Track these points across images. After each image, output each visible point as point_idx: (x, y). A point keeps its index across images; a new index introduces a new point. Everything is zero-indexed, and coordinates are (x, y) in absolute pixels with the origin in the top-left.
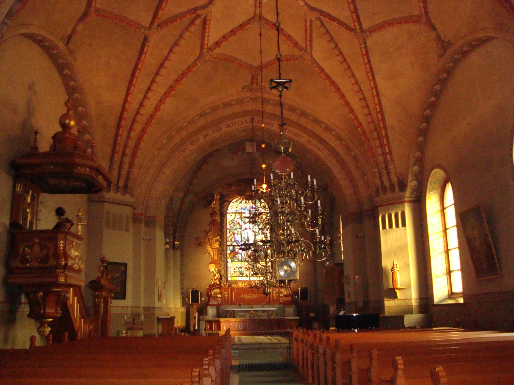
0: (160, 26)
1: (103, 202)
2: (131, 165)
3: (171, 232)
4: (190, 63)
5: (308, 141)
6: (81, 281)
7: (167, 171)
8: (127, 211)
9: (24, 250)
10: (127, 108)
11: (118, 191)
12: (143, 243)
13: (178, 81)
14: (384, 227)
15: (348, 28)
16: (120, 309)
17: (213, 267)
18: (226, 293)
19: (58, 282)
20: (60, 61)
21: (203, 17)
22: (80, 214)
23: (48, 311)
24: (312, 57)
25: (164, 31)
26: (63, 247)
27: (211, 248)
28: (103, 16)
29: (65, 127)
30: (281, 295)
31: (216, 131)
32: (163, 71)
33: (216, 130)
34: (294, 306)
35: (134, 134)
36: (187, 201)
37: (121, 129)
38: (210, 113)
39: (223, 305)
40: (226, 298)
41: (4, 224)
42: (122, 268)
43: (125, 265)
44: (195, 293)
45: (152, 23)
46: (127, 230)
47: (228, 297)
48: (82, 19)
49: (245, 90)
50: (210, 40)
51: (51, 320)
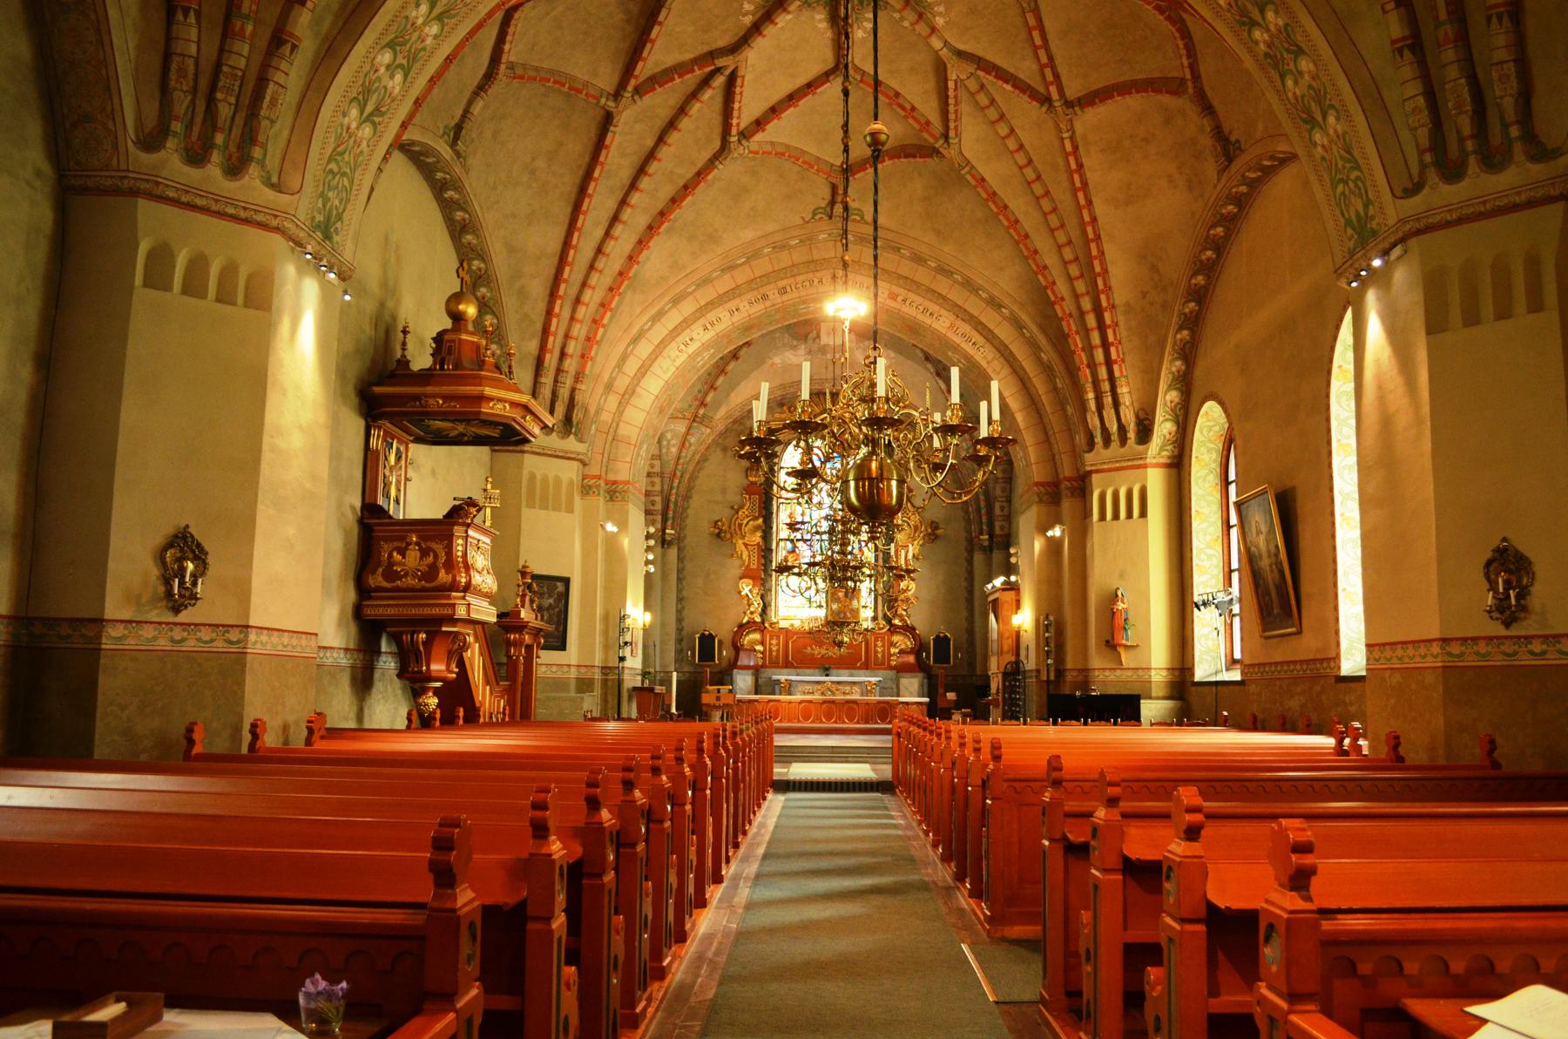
0: (639, 91)
3: (659, 507)
4: (700, 164)
5: (952, 325)
6: (486, 612)
9: (390, 556)
10: (570, 259)
13: (675, 201)
14: (1102, 517)
15: (1034, 95)
16: (554, 669)
17: (747, 586)
18: (774, 642)
19: (454, 614)
20: (439, 175)
21: (727, 72)
22: (489, 486)
23: (434, 667)
24: (961, 153)
25: (648, 100)
27: (746, 545)
28: (522, 77)
29: (457, 318)
30: (893, 650)
32: (645, 183)
34: (921, 675)
36: (693, 440)
37: (559, 302)
38: (743, 264)
39: (766, 667)
40: (774, 654)
41: (352, 507)
42: (560, 587)
43: (566, 581)
44: (707, 641)
45: (622, 85)
46: (570, 510)
47: (778, 650)
48: (481, 88)
49: (817, 217)
50: (743, 116)
51: (438, 684)
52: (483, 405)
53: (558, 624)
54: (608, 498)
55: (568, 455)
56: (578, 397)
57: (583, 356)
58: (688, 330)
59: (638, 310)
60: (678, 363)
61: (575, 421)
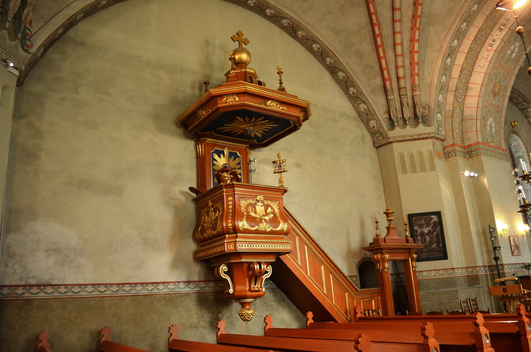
1: (391, 143)
8: (427, 146)
16: (442, 272)
26: (232, 209)
43: (438, 214)
46: (433, 169)
52: (219, 102)
53: (438, 242)
54: (468, 156)
55: (422, 136)
56: (417, 100)
58: (490, 36)
59: (444, 36)
60: (489, 59)
61: (419, 115)
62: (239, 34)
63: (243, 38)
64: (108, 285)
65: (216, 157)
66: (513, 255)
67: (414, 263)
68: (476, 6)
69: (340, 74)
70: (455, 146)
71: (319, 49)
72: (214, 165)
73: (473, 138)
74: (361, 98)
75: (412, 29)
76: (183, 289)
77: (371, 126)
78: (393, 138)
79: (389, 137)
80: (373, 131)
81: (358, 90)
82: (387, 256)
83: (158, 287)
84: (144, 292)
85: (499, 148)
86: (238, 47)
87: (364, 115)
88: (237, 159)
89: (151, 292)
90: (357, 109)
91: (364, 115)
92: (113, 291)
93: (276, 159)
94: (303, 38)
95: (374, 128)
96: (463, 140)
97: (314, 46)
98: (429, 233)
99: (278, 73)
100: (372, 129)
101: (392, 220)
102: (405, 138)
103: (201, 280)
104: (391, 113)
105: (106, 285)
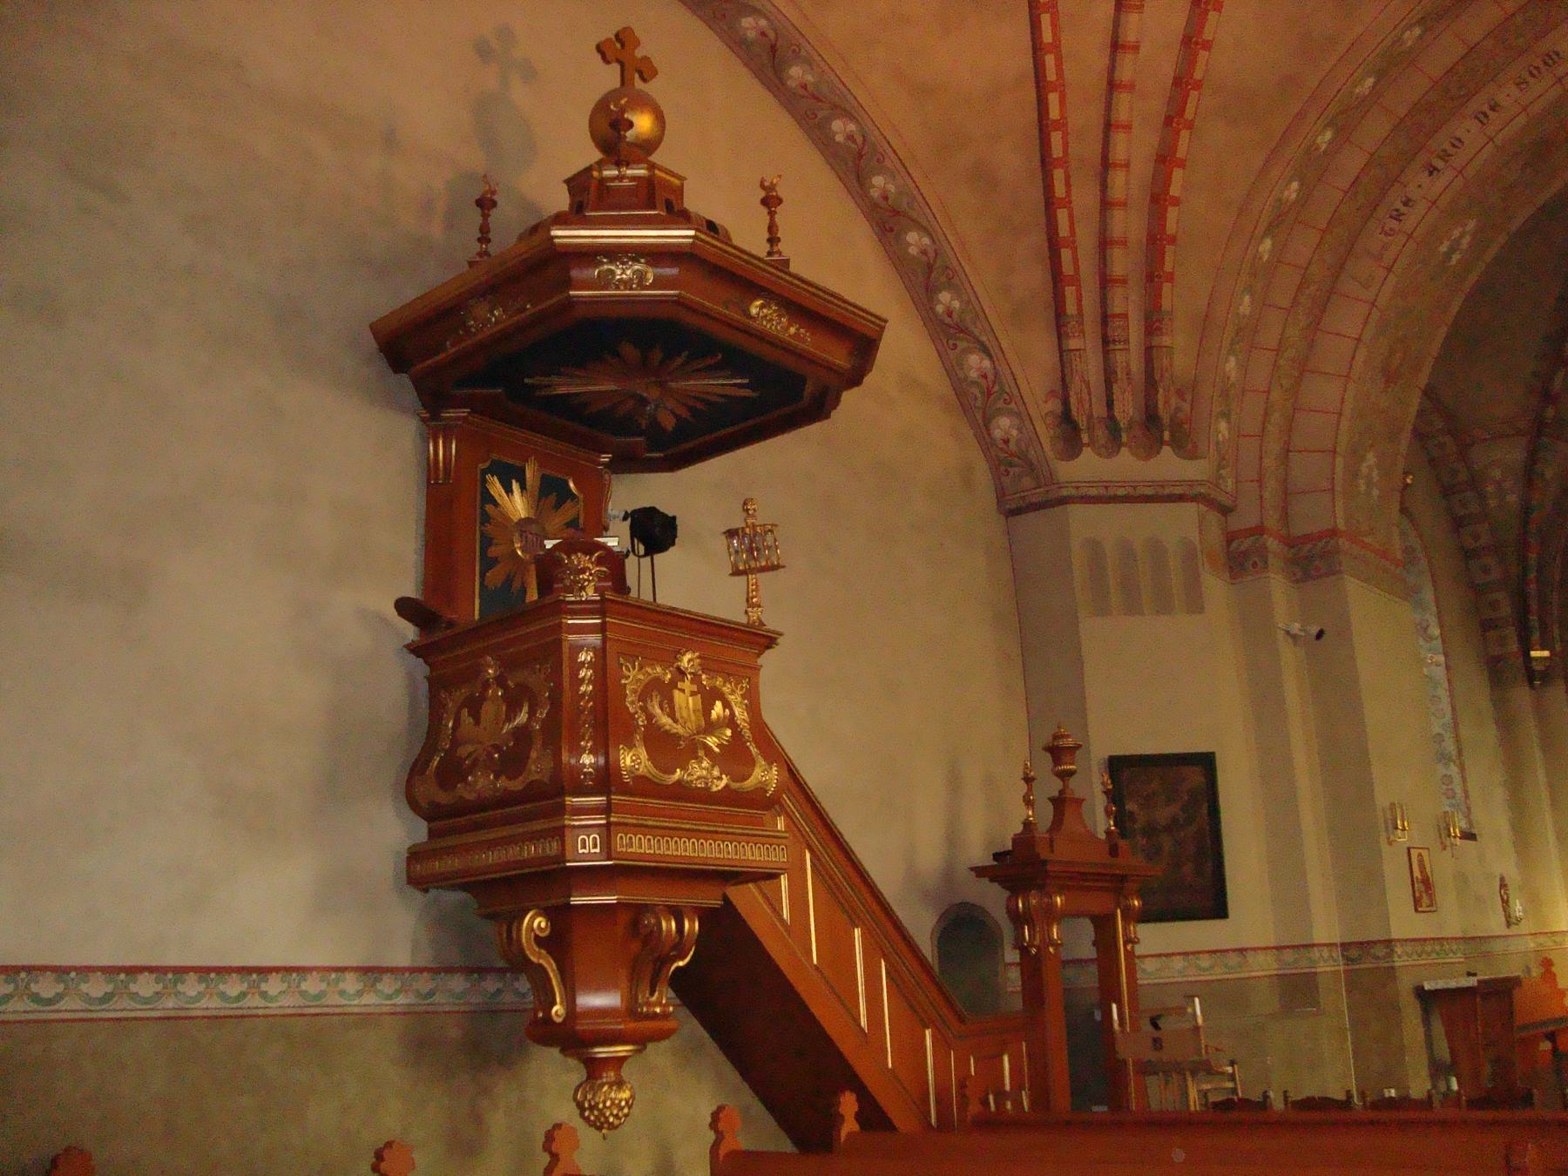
2: (1153, 324)
7: (1347, 320)
11: (1120, 445)
12: (1289, 656)
16: (1205, 962)
31: (1532, 75)
33: (1531, 73)
35: (1129, 184)
42: (1195, 777)
43: (1206, 762)
46: (1195, 604)
57: (1150, 277)
61: (1165, 415)
62: (624, 39)
63: (639, 53)
64: (73, 974)
65: (496, 487)
66: (1416, 910)
67: (1132, 928)
68: (1370, 81)
69: (912, 237)
70: (1265, 536)
71: (850, 137)
72: (486, 518)
73: (1310, 517)
74: (976, 332)
75: (1168, 121)
76: (352, 995)
77: (998, 434)
78: (1073, 487)
79: (1062, 480)
80: (1003, 455)
81: (969, 302)
82: (1059, 900)
83: (264, 987)
84: (212, 1004)
85: (1384, 555)
86: (618, 85)
87: (979, 395)
88: (569, 504)
89: (235, 1005)
90: (953, 372)
91: (979, 395)
92: (88, 999)
93: (737, 523)
94: (801, 92)
95: (1006, 442)
96: (1285, 516)
97: (837, 125)
98: (1172, 826)
99: (765, 202)
100: (1002, 445)
101: (1071, 773)
102: (1111, 492)
103: (422, 963)
104: (1073, 400)
105: (61, 971)
